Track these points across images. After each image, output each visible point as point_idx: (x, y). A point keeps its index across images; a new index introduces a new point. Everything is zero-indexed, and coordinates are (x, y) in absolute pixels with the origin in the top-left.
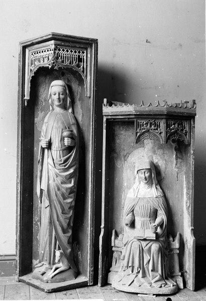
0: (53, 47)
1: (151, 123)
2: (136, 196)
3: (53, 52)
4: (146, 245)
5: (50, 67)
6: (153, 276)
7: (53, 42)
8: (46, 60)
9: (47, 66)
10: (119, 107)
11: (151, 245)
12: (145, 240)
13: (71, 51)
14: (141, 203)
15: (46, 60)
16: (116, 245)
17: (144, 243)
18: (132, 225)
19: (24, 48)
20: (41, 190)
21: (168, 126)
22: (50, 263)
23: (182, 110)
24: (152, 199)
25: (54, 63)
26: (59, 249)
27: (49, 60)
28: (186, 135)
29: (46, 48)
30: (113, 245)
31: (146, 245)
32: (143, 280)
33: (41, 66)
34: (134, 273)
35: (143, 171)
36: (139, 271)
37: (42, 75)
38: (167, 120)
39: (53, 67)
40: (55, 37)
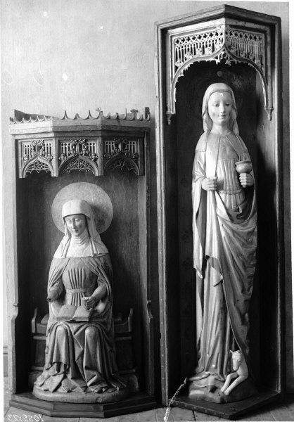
0: (222, 29)
1: (80, 145)
2: (64, 255)
3: (223, 36)
4: (78, 330)
5: (218, 61)
6: (88, 375)
7: (223, 20)
8: (208, 51)
9: (211, 59)
10: (33, 121)
11: (85, 329)
12: (73, 322)
13: (236, 35)
14: (70, 267)
15: (208, 51)
16: (39, 332)
17: (74, 327)
18: (61, 298)
19: (164, 32)
20: (205, 258)
21: (104, 147)
22: (221, 373)
23: (127, 124)
24: (87, 260)
25: (224, 55)
26: (237, 349)
27: (216, 51)
28: (136, 162)
29: (208, 31)
30: (33, 331)
31: (78, 330)
32: (74, 383)
33: (199, 60)
34: (61, 372)
35: (71, 218)
36: (68, 370)
37: (200, 75)
38: (104, 138)
39: (223, 61)
40: (232, 14)
